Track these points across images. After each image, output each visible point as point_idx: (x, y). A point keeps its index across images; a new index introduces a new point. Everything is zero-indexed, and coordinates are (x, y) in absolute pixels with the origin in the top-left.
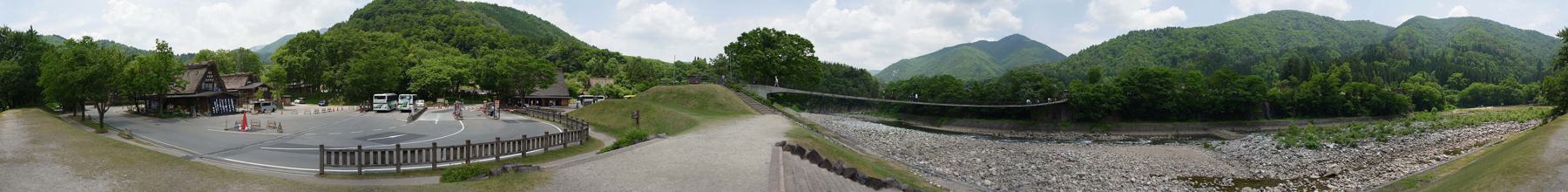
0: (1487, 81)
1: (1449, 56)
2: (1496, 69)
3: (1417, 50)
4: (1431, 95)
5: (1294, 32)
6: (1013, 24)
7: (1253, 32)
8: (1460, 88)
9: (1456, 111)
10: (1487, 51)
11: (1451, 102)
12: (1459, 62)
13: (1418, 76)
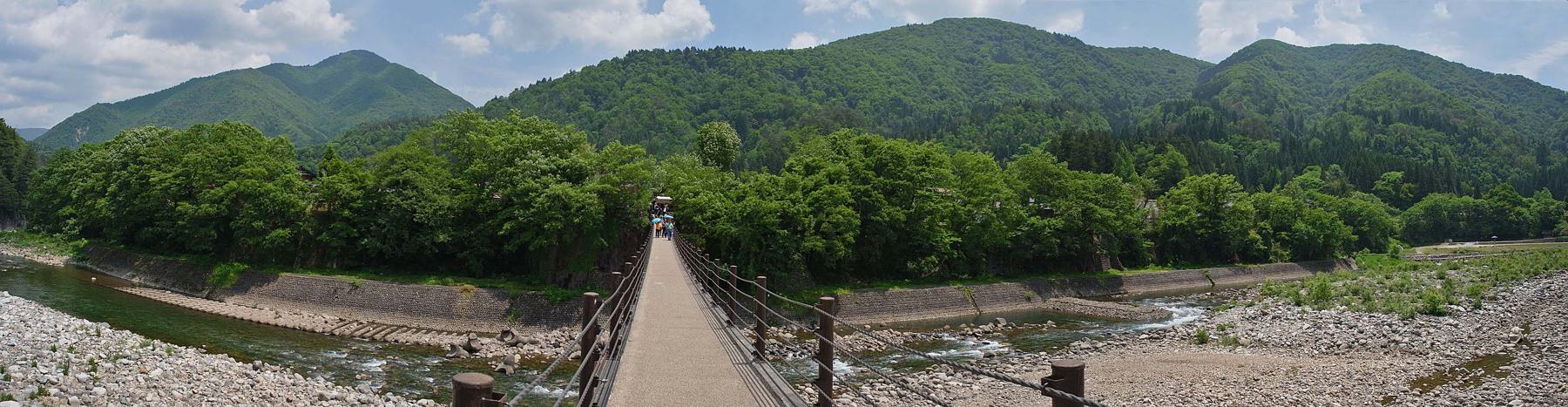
1: (1357, 133)
3: (1279, 116)
10: (1434, 123)
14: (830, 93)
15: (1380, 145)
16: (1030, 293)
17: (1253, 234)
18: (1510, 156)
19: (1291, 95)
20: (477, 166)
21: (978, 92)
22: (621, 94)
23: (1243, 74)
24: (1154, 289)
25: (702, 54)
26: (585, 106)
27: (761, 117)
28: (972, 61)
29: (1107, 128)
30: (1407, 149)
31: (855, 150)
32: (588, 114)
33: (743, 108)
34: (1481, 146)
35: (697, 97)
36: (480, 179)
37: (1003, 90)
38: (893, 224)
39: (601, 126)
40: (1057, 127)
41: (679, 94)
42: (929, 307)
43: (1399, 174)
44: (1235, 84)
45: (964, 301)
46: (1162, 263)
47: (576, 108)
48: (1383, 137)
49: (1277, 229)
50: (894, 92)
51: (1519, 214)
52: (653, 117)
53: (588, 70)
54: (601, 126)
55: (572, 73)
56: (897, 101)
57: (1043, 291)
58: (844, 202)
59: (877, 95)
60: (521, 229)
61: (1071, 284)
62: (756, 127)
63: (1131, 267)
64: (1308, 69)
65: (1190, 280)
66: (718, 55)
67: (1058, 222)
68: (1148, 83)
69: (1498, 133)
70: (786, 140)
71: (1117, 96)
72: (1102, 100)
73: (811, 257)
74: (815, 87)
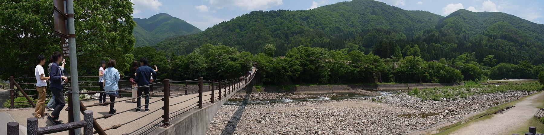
0: (510, 62)
1: (484, 42)
2: (517, 53)
3: (461, 35)
4: (474, 70)
5: (372, 17)
6: (459, 6)
7: (342, 15)
8: (492, 66)
9: (490, 81)
10: (511, 39)
11: (486, 74)
12: (491, 47)
13: (463, 56)
14: (316, 25)
15: (491, 46)
16: (349, 88)
17: (427, 74)
18: (536, 51)
19: (468, 28)
20: (211, 57)
21: (365, 25)
22: (249, 26)
23: (452, 21)
24: (388, 89)
25: (275, 12)
26: (237, 30)
27: (293, 33)
28: (364, 14)
29: (405, 38)
30: (500, 48)
31: (303, 51)
32: (238, 33)
33: (288, 30)
34: (526, 47)
35: (273, 27)
36: (212, 61)
37: (373, 24)
38: (311, 69)
39: (242, 37)
40: (387, 38)
41: (268, 26)
42: (320, 90)
43: (492, 56)
44: (449, 24)
45: (329, 89)
46: (395, 82)
47: (234, 31)
48: (492, 43)
49: (435, 73)
50: (337, 25)
51: (529, 71)
52: (259, 33)
53: (238, 18)
54: (242, 37)
55: (233, 19)
56: (338, 28)
57: (353, 88)
58: (297, 64)
59: (331, 26)
60: (222, 72)
61: (362, 87)
62: (291, 37)
63: (385, 82)
64: (475, 20)
65: (401, 87)
66: (280, 12)
67: (358, 69)
68: (421, 23)
69: (533, 44)
70: (301, 41)
71: (411, 27)
72: (405, 28)
73: (290, 77)
74: (312, 23)
